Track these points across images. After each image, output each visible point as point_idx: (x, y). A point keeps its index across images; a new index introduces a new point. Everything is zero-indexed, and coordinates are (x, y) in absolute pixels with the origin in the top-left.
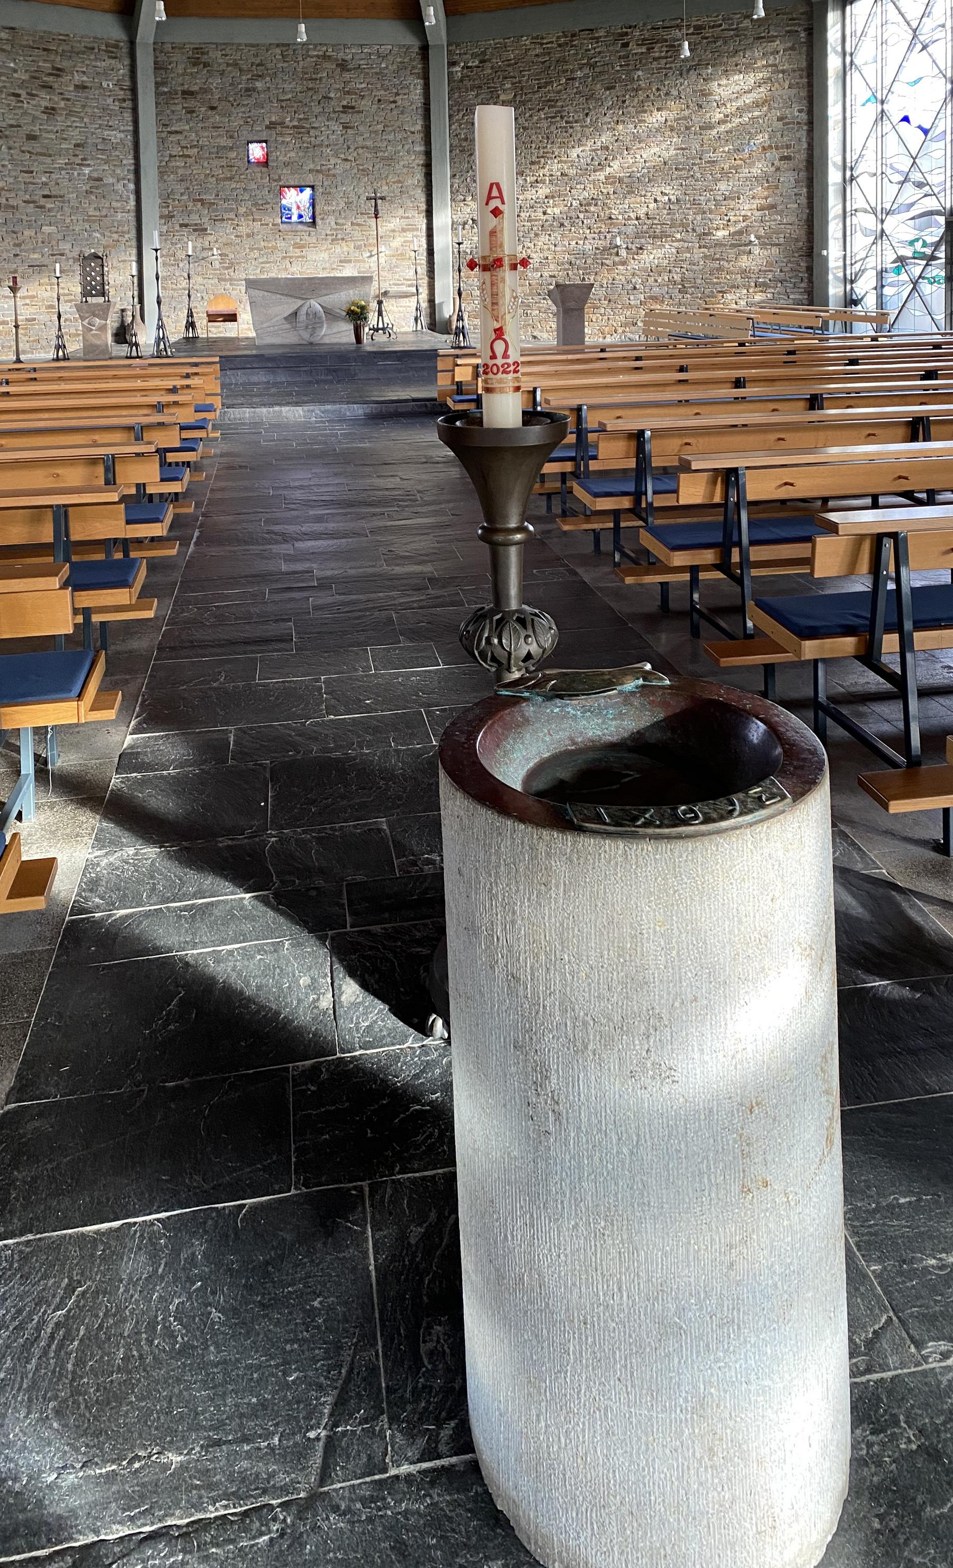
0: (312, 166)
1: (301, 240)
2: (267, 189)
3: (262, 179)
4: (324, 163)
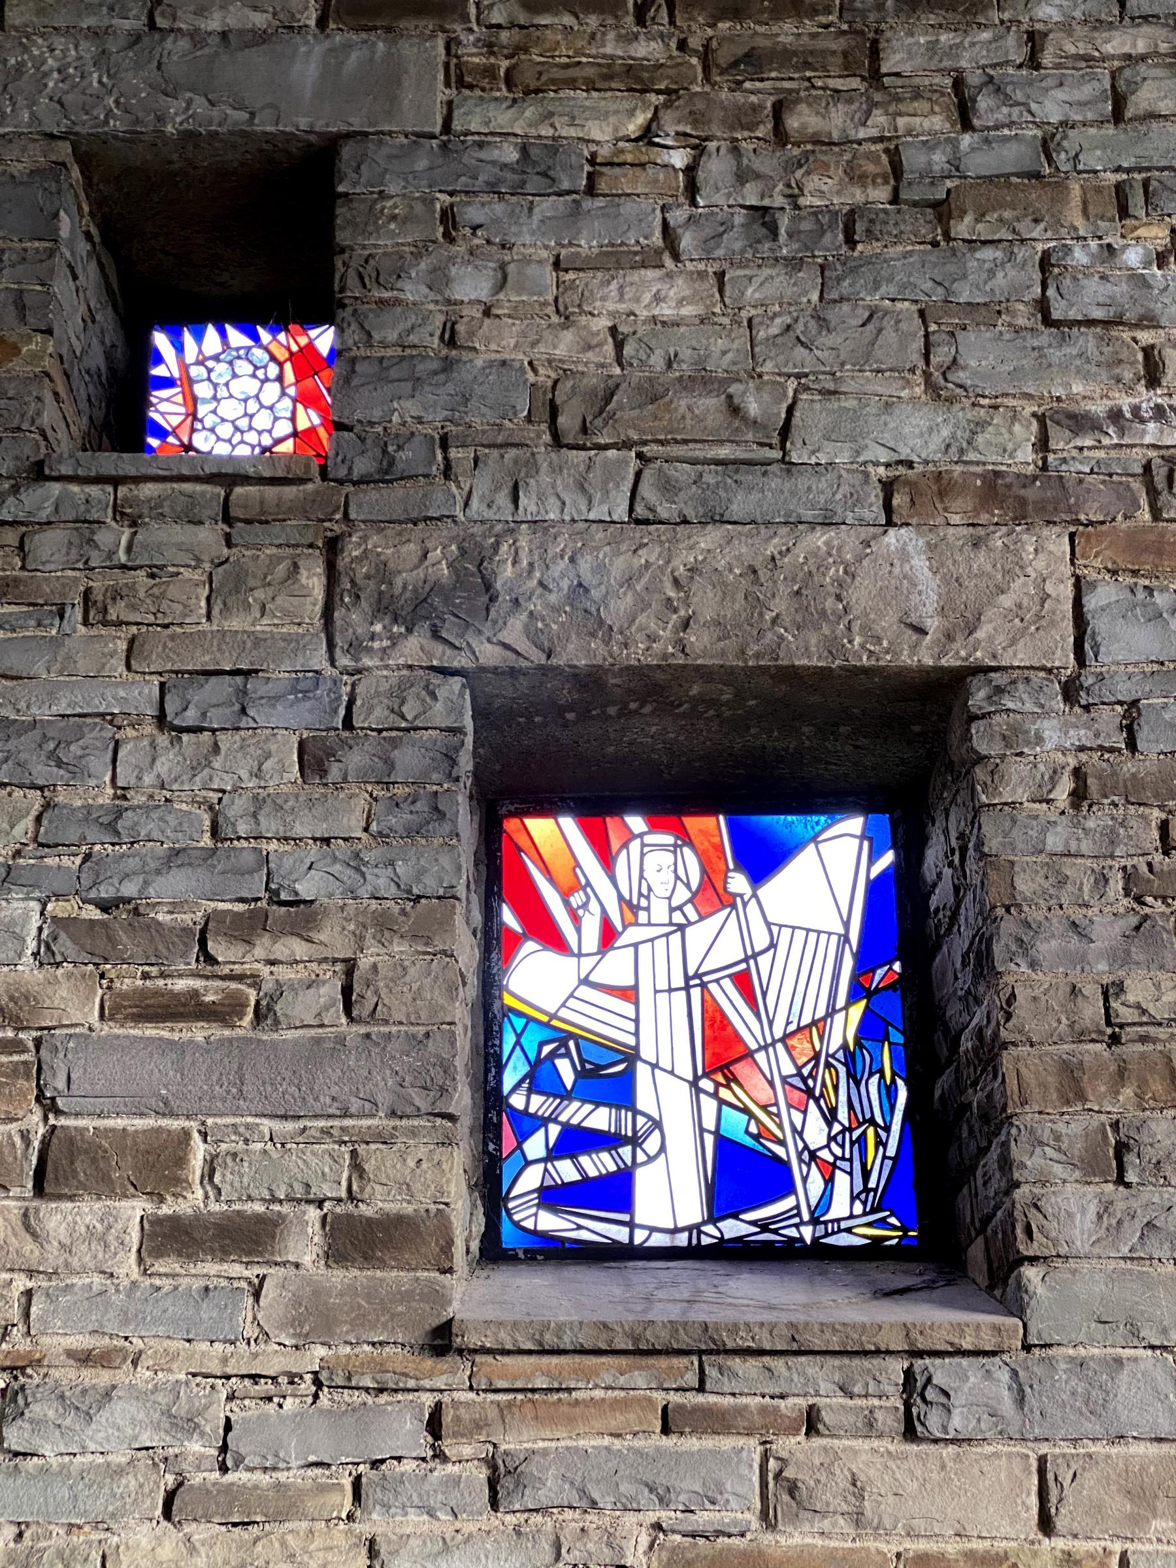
0: (919, 433)
1: (781, 1494)
2: (282, 729)
3: (227, 588)
4: (1089, 393)
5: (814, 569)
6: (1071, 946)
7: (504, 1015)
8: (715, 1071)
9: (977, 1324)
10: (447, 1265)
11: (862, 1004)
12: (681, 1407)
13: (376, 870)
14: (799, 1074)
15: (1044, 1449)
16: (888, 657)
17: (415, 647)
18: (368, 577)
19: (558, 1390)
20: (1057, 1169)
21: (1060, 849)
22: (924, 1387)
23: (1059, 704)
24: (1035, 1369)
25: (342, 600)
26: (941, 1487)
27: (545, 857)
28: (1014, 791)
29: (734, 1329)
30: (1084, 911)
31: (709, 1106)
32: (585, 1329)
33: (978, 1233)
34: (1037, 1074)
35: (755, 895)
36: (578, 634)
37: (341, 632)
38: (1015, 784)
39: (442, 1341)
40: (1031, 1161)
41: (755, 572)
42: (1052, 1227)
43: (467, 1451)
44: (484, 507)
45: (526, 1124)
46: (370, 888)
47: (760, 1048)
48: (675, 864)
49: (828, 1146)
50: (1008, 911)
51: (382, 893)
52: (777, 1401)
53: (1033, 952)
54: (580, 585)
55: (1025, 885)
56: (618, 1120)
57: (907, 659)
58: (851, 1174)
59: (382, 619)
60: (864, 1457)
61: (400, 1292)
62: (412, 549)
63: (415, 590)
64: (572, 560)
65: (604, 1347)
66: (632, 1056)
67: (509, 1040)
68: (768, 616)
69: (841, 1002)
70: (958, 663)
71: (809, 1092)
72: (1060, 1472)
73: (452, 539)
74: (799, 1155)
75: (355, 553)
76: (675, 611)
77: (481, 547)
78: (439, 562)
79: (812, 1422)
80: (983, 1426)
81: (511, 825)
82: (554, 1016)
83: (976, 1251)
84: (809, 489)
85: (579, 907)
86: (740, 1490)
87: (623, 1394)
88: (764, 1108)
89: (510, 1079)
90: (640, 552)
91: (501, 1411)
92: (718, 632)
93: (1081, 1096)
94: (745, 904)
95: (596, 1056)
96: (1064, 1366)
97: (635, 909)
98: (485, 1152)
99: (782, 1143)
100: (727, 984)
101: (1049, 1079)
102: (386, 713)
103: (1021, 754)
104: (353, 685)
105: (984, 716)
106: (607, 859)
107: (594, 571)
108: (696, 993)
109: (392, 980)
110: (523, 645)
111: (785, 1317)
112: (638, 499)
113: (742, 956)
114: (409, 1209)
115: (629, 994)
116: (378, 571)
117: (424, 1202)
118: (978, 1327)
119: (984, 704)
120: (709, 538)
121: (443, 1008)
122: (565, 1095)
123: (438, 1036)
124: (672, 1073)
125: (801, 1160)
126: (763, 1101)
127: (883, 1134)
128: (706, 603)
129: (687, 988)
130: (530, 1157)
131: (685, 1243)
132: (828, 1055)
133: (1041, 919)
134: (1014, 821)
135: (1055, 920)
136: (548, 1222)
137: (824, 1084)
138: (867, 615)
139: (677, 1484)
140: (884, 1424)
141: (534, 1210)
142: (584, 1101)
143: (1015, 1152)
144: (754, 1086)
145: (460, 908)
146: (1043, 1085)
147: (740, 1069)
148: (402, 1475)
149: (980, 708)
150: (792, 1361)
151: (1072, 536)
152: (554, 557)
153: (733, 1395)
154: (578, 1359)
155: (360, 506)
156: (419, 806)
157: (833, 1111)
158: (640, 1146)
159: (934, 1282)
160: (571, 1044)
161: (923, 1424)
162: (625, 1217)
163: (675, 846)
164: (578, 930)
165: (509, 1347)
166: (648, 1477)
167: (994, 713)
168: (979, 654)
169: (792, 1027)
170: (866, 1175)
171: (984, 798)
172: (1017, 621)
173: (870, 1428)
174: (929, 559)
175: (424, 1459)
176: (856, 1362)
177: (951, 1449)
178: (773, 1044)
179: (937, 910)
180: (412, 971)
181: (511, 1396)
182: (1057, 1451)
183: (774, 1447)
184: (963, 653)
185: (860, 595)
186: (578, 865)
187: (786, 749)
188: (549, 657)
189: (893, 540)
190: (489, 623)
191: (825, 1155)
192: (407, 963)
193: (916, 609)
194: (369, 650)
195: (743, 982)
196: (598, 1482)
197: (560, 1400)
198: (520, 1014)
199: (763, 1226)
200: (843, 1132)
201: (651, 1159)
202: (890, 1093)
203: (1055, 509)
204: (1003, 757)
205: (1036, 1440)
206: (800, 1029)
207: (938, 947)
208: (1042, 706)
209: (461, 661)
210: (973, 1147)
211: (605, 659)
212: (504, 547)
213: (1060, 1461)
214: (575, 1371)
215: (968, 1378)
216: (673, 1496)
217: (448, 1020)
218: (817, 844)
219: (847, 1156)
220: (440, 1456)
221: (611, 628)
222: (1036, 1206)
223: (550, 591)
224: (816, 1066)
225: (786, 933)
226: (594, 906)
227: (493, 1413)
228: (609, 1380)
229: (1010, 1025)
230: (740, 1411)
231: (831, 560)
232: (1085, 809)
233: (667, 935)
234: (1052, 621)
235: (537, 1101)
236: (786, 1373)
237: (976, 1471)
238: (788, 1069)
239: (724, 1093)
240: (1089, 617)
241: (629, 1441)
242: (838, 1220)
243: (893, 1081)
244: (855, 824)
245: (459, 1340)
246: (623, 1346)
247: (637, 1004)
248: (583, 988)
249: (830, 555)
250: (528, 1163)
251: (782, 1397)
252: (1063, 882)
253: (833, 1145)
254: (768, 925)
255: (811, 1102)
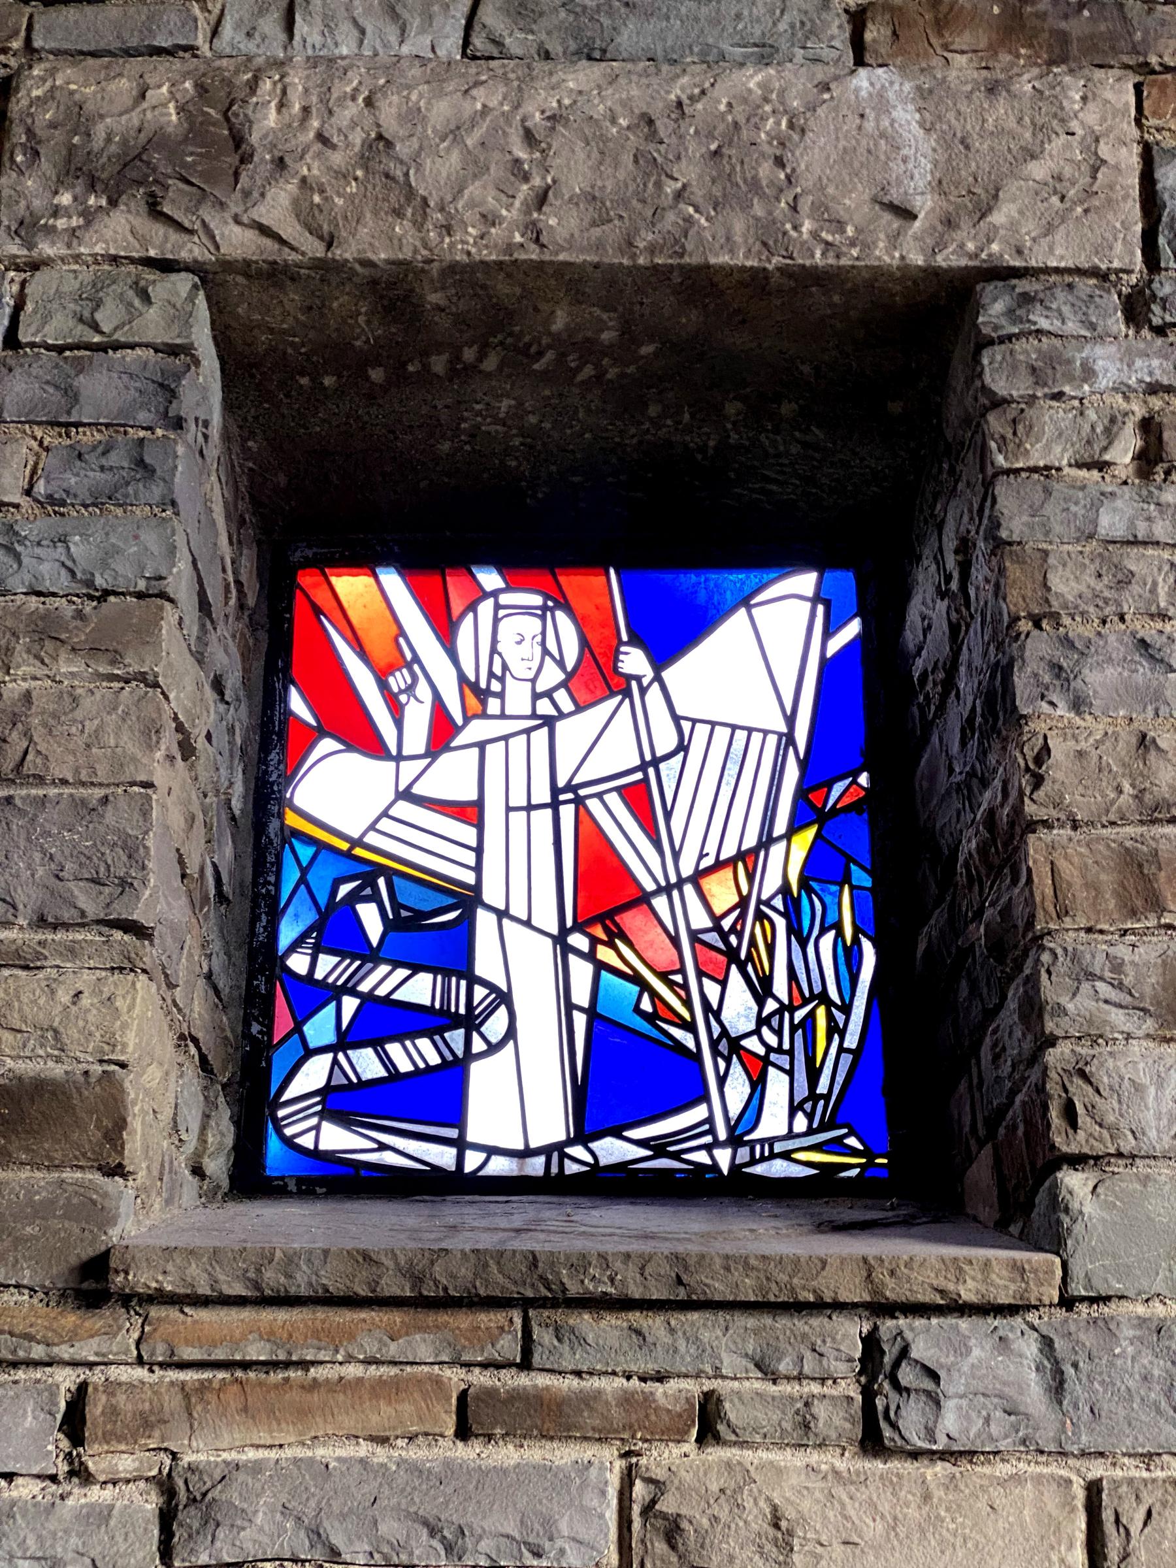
5: (742, 120)
6: (1139, 678)
7: (284, 841)
8: (592, 922)
9: (987, 1267)
10: (113, 1161)
11: (810, 834)
12: (490, 1394)
13: (38, 550)
14: (717, 928)
15: (1097, 1470)
16: (855, 252)
17: (122, 229)
18: (53, 125)
19: (287, 1365)
20: (1117, 1017)
21: (1120, 532)
22: (896, 1365)
23: (1117, 322)
24: (1082, 1336)
25: (12, 160)
26: (923, 1532)
27: (345, 604)
28: (1048, 448)
29: (579, 1264)
30: (1159, 625)
31: (582, 972)
32: (333, 1263)
33: (981, 1144)
34: (1084, 869)
35: (658, 678)
36: (375, 213)
37: (9, 206)
38: (1050, 440)
39: (93, 1284)
40: (1072, 1003)
41: (651, 122)
42: (1109, 1108)
43: (126, 1464)
44: (240, 37)
45: (313, 995)
46: (27, 578)
47: (659, 891)
48: (544, 633)
49: (757, 1032)
50: (1037, 625)
51: (47, 586)
52: (650, 1386)
53: (1077, 684)
54: (380, 137)
55: (1066, 585)
56: (446, 991)
57: (884, 255)
58: (790, 1073)
59: (73, 186)
60: (794, 1481)
61: (30, 1203)
62: (124, 86)
63: (124, 142)
64: (369, 102)
65: (363, 1291)
66: (469, 899)
67: (291, 876)
68: (670, 188)
69: (780, 827)
70: (964, 262)
71: (732, 955)
72: (1125, 1508)
73: (185, 75)
74: (714, 1044)
75: (36, 93)
76: (526, 178)
77: (228, 83)
78: (165, 105)
79: (708, 1421)
80: (994, 1429)
81: (306, 579)
82: (358, 843)
83: (981, 1172)
84: (738, 16)
85: (401, 692)
86: (583, 1534)
87: (393, 1371)
88: (664, 976)
89: (287, 933)
90: (474, 92)
91: (187, 1397)
92: (592, 213)
93: (1156, 904)
94: (643, 691)
95: (413, 897)
96: (1131, 1333)
97: (483, 695)
98: (247, 1035)
99: (691, 1027)
100: (613, 800)
101: (1103, 877)
102: (71, 323)
103: (1058, 396)
104: (23, 284)
105: (1002, 340)
106: (445, 629)
107: (401, 118)
108: (567, 813)
109: (54, 715)
110: (290, 230)
111: (666, 1248)
112: (477, 27)
113: (638, 762)
114: (57, 1071)
115: (470, 812)
116: (68, 116)
117: (82, 1059)
118: (987, 1264)
119: (1003, 321)
120: (581, 76)
121: (134, 759)
122: (369, 955)
123: (122, 803)
124: (528, 923)
125: (716, 1053)
126: (662, 967)
127: (840, 1017)
128: (574, 168)
129: (555, 805)
130: (313, 1043)
131: (540, 1172)
132: (759, 902)
133: (1092, 635)
134: (1048, 492)
135: (1112, 638)
136: (336, 1138)
137: (753, 943)
138: (823, 189)
139: (476, 1522)
140: (829, 1423)
141: (314, 1121)
142: (396, 964)
143: (1049, 990)
144: (646, 944)
145: (170, 615)
146: (1093, 887)
147: (631, 920)
148: (13, 1503)
149: (996, 328)
150: (677, 1319)
151: (1138, 88)
152: (341, 99)
153: (578, 1374)
154: (321, 1313)
155: (49, 30)
156: (113, 459)
157: (767, 981)
158: (478, 1028)
159: (914, 1217)
160: (381, 881)
161: (894, 1426)
162: (453, 1133)
163: (544, 608)
164: (399, 723)
165: (204, 1290)
166: (428, 1510)
167: (1017, 336)
168: (995, 247)
169: (708, 862)
170: (814, 1075)
171: (1000, 460)
172: (1055, 200)
173: (804, 1431)
174: (919, 110)
175: (53, 1478)
176: (783, 1323)
177: (941, 1468)
178: (681, 882)
179: (924, 675)
180: (87, 702)
181: (206, 1375)
182: (1119, 1473)
183: (643, 1461)
184: (970, 246)
185: (814, 158)
186: (401, 632)
187: (703, 449)
188: (329, 246)
189: (865, 84)
190: (238, 194)
191: (752, 1044)
192: (79, 691)
193: (899, 183)
194: (50, 230)
195: (638, 798)
196: (343, 1517)
197: (287, 1380)
198: (310, 840)
199: (658, 1146)
200: (779, 1012)
201: (493, 1048)
202: (850, 958)
203: (1113, 48)
204: (1032, 400)
205: (1084, 1454)
206: (718, 865)
207: (925, 740)
208: (1093, 327)
209: (193, 250)
210: (976, 1010)
211: (416, 251)
212: (266, 85)
213: (1124, 1489)
214: (316, 1334)
215: (969, 1351)
216: (469, 1542)
217: (142, 777)
218: (749, 608)
219: (786, 1046)
220: (80, 1474)
221: (425, 201)
222: (1082, 1074)
223: (334, 147)
224: (742, 917)
225: (702, 731)
226: (423, 690)
227: (173, 1402)
228: (371, 1347)
229: (1040, 794)
230: (589, 1400)
231: (768, 108)
232: (1159, 477)
233: (528, 731)
234: (1109, 201)
235: (326, 963)
236: (668, 1340)
237: (982, 1505)
238: (700, 920)
239: (605, 954)
240: (1166, 197)
241: (403, 1451)
242: (771, 1141)
243: (856, 941)
244: (805, 582)
245: (120, 1278)
246: (396, 1291)
247: (480, 827)
248: (402, 804)
249: (766, 100)
250: (310, 1052)
251: (660, 1378)
252: (1125, 580)
253: (765, 1031)
254: (676, 719)
255: (734, 967)
